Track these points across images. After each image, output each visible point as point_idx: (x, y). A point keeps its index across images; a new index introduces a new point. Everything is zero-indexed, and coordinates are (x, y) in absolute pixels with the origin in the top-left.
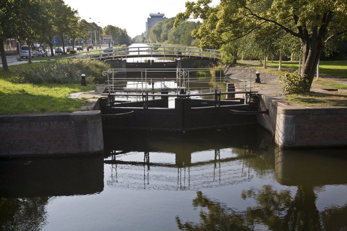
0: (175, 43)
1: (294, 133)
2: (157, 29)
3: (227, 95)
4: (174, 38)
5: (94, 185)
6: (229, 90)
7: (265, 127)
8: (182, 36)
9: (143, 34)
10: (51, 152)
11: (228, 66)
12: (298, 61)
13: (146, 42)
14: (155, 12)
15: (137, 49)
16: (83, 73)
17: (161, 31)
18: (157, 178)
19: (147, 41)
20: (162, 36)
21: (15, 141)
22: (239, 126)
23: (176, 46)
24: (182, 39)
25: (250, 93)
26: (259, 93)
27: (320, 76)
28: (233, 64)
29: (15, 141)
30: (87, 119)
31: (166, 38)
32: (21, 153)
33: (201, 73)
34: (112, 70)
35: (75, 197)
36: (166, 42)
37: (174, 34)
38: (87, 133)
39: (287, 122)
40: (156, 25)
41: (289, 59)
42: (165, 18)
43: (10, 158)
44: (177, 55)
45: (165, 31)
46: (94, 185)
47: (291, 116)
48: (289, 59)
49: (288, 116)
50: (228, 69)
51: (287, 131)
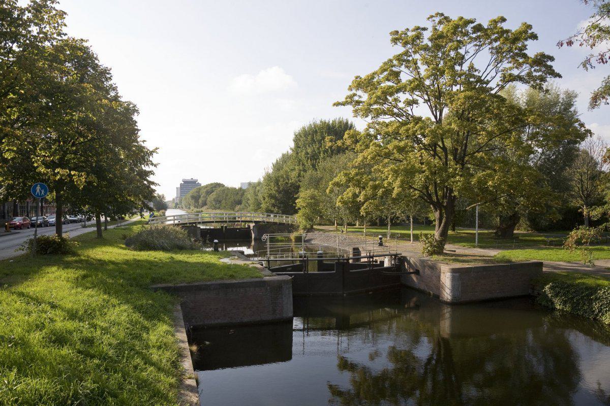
0: (215, 208)
1: (460, 290)
2: (195, 194)
3: (317, 261)
4: (214, 203)
5: (283, 353)
6: (354, 255)
7: (414, 286)
8: (223, 201)
9: (174, 199)
10: (245, 320)
11: (305, 232)
12: (363, 227)
13: (179, 208)
14: (188, 178)
15: (172, 218)
16: (216, 239)
17: (200, 197)
18: (313, 343)
19: (180, 206)
20: (200, 201)
21: (211, 309)
22: (389, 290)
23: (218, 211)
24: (224, 205)
25: (396, 255)
26: (403, 255)
27: (414, 240)
28: (310, 230)
29: (211, 309)
30: (283, 284)
31: (205, 204)
32: (216, 322)
33: (279, 238)
34: (267, 235)
35: (228, 371)
36: (205, 207)
37: (214, 200)
38: (282, 298)
39: (453, 279)
40: (193, 191)
41: (355, 225)
42: (198, 183)
43: (206, 327)
44: (227, 220)
45: (204, 197)
46: (283, 353)
47: (457, 274)
48: (355, 225)
49: (455, 274)
50: (306, 235)
51: (454, 288)
